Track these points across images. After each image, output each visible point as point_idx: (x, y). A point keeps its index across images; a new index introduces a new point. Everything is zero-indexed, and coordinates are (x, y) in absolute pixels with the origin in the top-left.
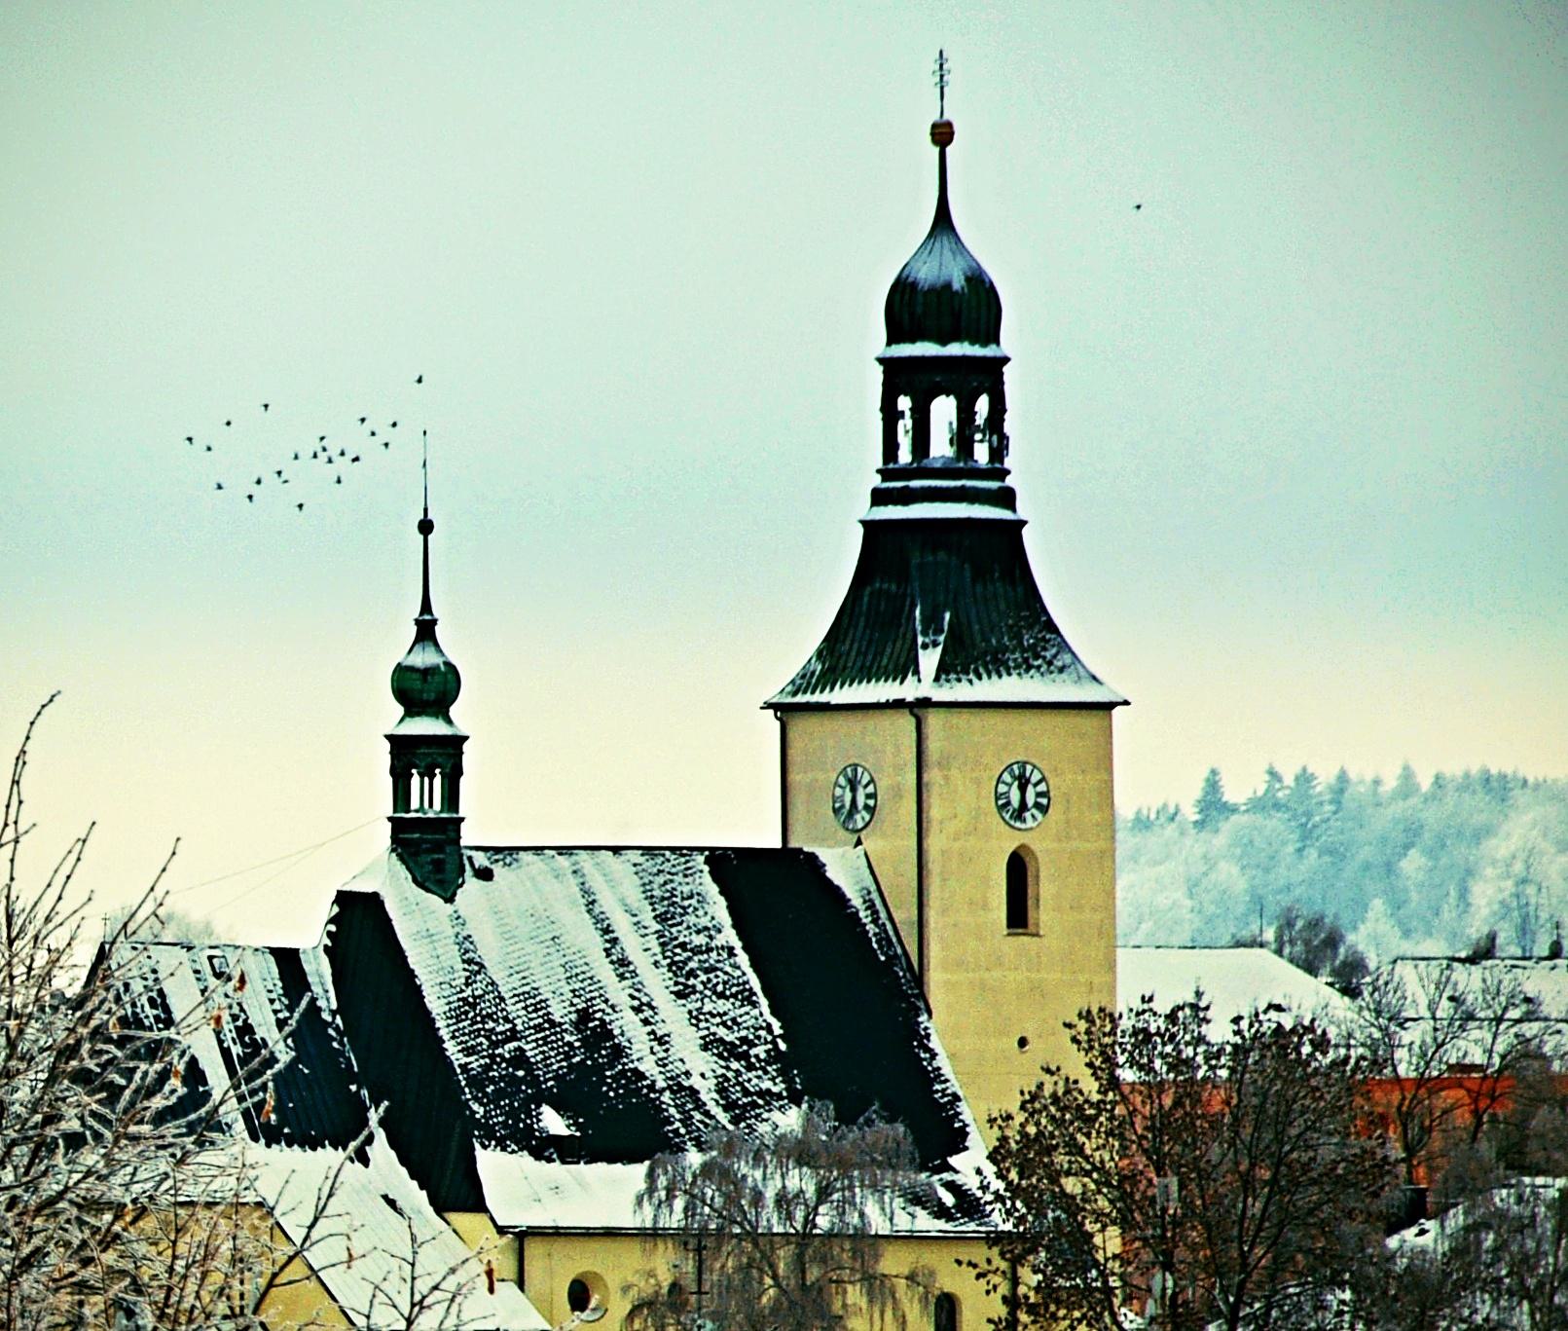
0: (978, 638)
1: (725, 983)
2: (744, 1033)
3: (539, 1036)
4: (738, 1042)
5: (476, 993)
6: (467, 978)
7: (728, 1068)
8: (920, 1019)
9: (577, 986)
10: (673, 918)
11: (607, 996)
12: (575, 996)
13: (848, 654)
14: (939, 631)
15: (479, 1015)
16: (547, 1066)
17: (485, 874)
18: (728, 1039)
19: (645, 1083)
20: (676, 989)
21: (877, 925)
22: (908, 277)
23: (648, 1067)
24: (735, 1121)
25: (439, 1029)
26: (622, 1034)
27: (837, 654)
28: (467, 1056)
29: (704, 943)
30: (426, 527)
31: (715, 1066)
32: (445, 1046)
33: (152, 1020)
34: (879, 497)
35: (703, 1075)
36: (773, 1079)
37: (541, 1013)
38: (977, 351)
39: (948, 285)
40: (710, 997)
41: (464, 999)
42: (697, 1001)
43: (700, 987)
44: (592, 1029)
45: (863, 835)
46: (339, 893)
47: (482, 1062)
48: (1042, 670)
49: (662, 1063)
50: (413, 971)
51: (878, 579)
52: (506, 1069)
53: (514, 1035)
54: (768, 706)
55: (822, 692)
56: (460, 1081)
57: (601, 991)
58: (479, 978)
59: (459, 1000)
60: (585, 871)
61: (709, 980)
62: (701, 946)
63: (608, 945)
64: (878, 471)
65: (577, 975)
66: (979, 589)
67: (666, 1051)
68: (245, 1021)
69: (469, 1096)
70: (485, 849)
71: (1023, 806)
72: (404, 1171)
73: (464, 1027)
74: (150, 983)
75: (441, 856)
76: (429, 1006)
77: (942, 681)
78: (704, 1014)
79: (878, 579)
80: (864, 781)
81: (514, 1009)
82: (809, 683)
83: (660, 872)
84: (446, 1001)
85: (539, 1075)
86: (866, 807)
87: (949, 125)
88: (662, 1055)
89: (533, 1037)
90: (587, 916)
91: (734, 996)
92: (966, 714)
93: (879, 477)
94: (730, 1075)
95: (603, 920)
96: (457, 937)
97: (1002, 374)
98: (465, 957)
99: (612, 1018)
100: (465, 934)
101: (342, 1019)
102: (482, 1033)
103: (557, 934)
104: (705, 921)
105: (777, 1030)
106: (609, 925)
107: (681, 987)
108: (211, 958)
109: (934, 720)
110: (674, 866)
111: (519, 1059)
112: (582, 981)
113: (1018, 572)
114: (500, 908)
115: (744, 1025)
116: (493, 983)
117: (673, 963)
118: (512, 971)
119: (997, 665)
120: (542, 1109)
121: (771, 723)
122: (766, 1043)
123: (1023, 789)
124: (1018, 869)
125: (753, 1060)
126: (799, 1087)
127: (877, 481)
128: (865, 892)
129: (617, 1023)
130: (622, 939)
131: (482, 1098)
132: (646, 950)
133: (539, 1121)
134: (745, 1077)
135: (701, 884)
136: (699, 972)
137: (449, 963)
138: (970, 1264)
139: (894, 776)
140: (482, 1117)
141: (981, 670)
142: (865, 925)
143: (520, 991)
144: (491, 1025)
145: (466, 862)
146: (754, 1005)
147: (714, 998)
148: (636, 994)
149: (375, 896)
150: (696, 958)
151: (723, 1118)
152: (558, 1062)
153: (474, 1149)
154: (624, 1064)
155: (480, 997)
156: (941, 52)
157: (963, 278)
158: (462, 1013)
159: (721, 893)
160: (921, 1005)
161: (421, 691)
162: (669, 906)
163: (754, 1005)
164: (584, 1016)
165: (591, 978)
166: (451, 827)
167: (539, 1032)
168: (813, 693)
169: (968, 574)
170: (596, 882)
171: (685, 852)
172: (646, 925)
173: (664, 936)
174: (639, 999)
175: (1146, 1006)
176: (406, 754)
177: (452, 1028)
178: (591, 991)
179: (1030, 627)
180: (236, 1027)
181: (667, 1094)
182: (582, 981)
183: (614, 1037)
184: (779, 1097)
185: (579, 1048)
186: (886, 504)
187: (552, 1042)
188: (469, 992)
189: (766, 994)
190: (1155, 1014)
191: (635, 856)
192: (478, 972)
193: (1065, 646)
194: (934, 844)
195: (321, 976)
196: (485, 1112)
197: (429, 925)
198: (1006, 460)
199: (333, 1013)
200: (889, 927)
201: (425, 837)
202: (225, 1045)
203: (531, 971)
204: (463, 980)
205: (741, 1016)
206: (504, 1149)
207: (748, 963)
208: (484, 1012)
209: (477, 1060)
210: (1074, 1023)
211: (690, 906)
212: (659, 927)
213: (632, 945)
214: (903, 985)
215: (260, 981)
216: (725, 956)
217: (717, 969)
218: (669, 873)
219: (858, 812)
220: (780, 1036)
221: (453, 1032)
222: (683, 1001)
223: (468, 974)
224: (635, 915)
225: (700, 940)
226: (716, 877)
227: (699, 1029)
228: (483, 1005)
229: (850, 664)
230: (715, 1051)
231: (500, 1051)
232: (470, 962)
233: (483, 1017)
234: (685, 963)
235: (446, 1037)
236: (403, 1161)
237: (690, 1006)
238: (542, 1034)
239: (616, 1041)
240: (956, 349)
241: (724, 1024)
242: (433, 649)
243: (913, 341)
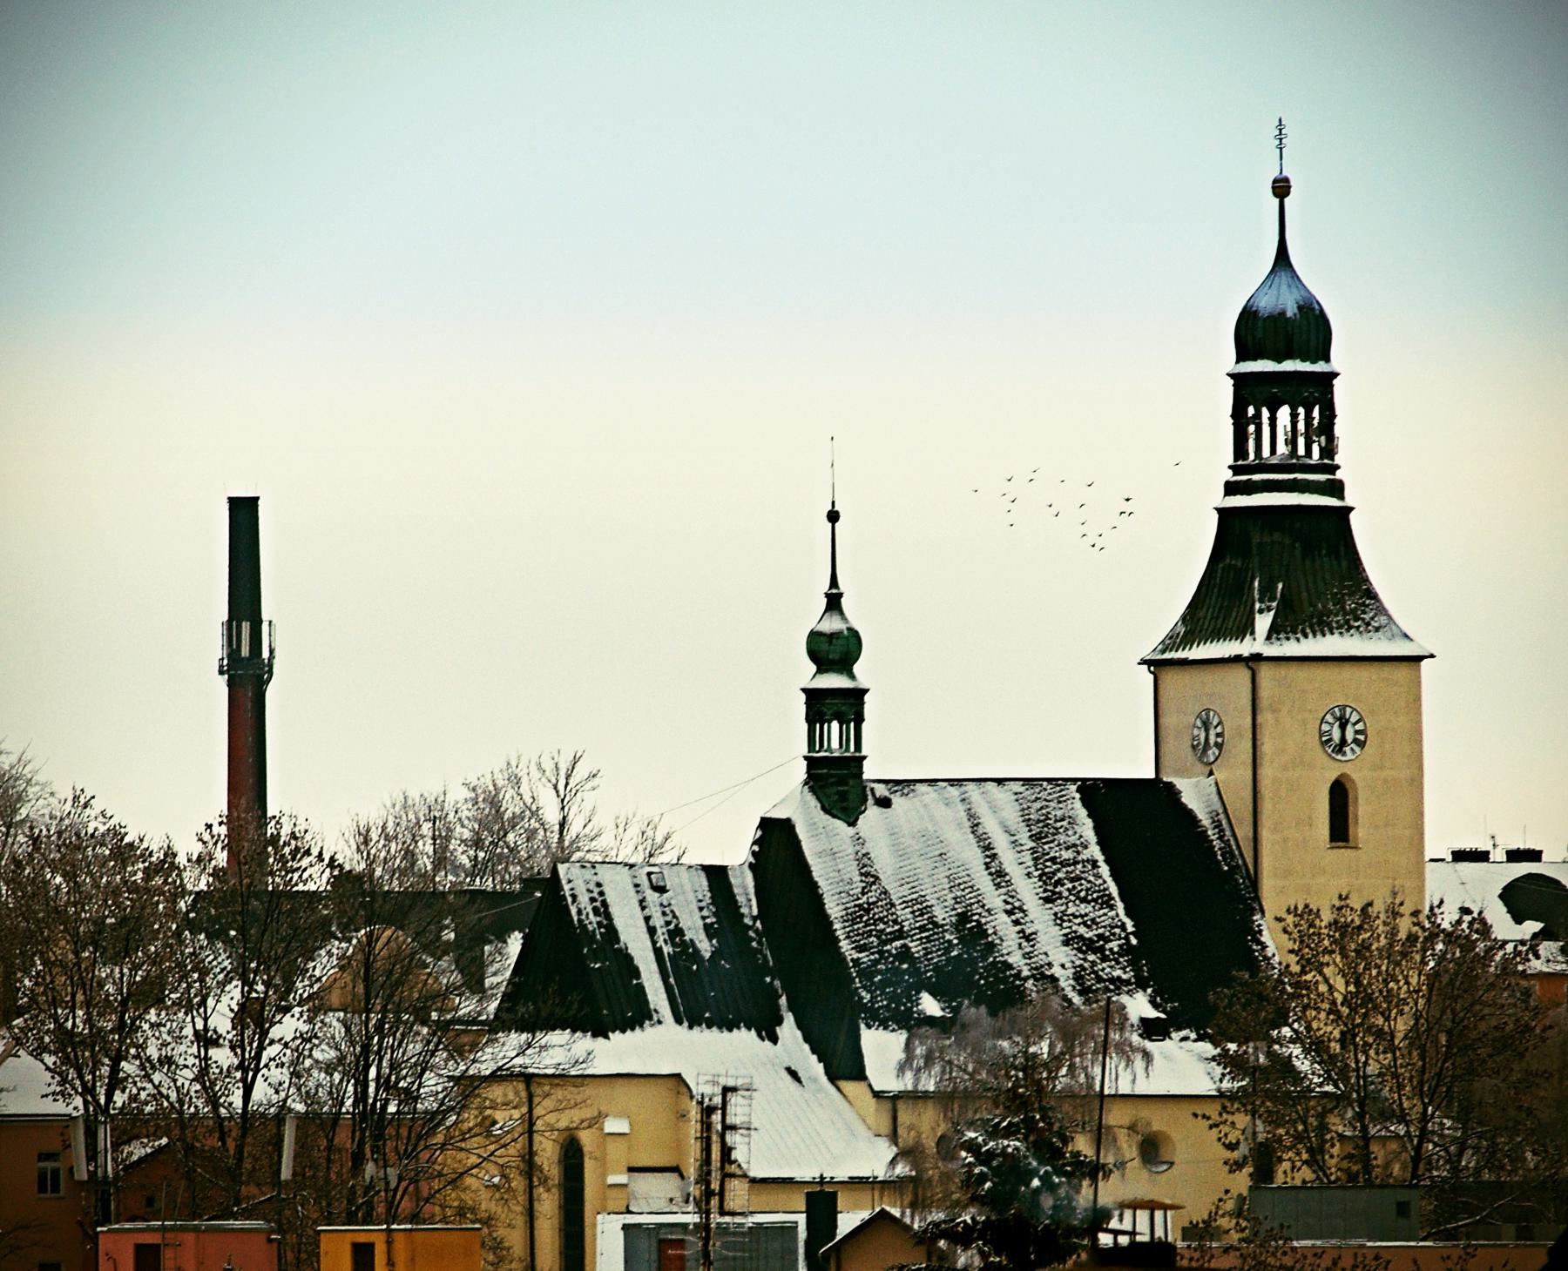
0: (1306, 604)
1: (1087, 890)
2: (1101, 931)
3: (923, 935)
4: (1095, 939)
5: (871, 900)
6: (864, 888)
7: (1085, 960)
8: (1255, 918)
9: (959, 894)
10: (1046, 836)
11: (985, 902)
12: (957, 903)
13: (1205, 618)
14: (1272, 599)
15: (872, 918)
16: (928, 960)
17: (884, 803)
18: (1087, 936)
19: (1012, 972)
20: (1045, 895)
21: (1223, 841)
22: (1252, 306)
23: (1016, 959)
24: (1087, 1002)
25: (836, 930)
26: (995, 933)
27: (1195, 620)
28: (860, 952)
29: (1071, 857)
30: (833, 517)
31: (1074, 959)
32: (841, 944)
33: (595, 926)
34: (1231, 489)
35: (1063, 966)
36: (1123, 969)
37: (926, 917)
38: (1306, 367)
39: (1283, 313)
40: (1074, 902)
41: (859, 906)
42: (1062, 905)
43: (1066, 894)
44: (971, 929)
45: (1213, 767)
46: (763, 819)
47: (872, 957)
48: (1361, 629)
49: (1027, 956)
50: (816, 883)
51: (1228, 556)
52: (893, 962)
53: (900, 934)
54: (1144, 662)
55: (1183, 649)
56: (851, 973)
57: (980, 898)
58: (874, 887)
59: (855, 906)
60: (972, 799)
61: (1074, 887)
62: (1069, 860)
63: (988, 860)
64: (1230, 467)
65: (960, 884)
66: (1308, 563)
67: (1033, 946)
68: (677, 925)
69: (858, 985)
70: (886, 782)
71: (1343, 741)
72: (807, 1047)
73: (859, 929)
74: (595, 895)
75: (846, 788)
76: (829, 911)
77: (1273, 640)
78: (1068, 915)
79: (1228, 556)
80: (1215, 723)
81: (904, 914)
82: (1175, 642)
83: (1037, 799)
84: (844, 907)
85: (920, 967)
86: (1216, 744)
87: (1286, 180)
88: (1028, 949)
89: (918, 936)
90: (972, 836)
91: (1095, 900)
92: (1294, 666)
93: (1230, 472)
94: (1086, 965)
95: (986, 839)
96: (857, 853)
97: (1333, 386)
98: (863, 871)
99: (988, 919)
100: (864, 851)
101: (762, 923)
102: (874, 933)
103: (943, 851)
104: (1073, 839)
105: (1130, 928)
106: (990, 843)
107: (1050, 894)
108: (649, 874)
109: (1266, 673)
110: (1050, 794)
111: (905, 954)
112: (963, 890)
113: (1342, 548)
114: (896, 830)
115: (1103, 924)
116: (885, 893)
117: (1044, 874)
118: (903, 882)
119: (1321, 626)
120: (921, 995)
121: (1146, 677)
122: (1120, 939)
123: (1343, 727)
124: (1340, 794)
125: (1107, 953)
126: (1146, 974)
127: (1228, 475)
128: (1214, 813)
129: (993, 924)
130: (1000, 854)
131: (871, 986)
132: (1021, 864)
133: (918, 1005)
134: (1100, 967)
135: (1072, 809)
136: (1066, 881)
137: (848, 876)
138: (1204, 1116)
139: (1237, 720)
140: (869, 1002)
141: (1308, 631)
142: (1213, 841)
143: (910, 898)
144: (881, 926)
145: (869, 793)
146: (1112, 907)
147: (1077, 902)
148: (1010, 900)
149: (788, 820)
150: (1064, 870)
151: (1077, 1000)
152: (939, 956)
153: (859, 1029)
154: (995, 957)
155: (874, 903)
156: (1280, 120)
157: (1295, 306)
158: (858, 917)
159: (1089, 816)
160: (1256, 906)
161: (828, 652)
162: (1043, 827)
163: (1112, 907)
164: (964, 918)
165: (972, 887)
166: (853, 764)
167: (924, 932)
168: (1177, 651)
169: (1298, 552)
170: (982, 809)
171: (1060, 782)
172: (1023, 842)
173: (1036, 852)
174: (1012, 904)
175: (1343, 903)
176: (820, 706)
177: (848, 929)
178: (971, 898)
179: (1352, 594)
180: (668, 931)
181: (1031, 981)
182: (963, 890)
183: (988, 935)
184: (1128, 982)
185: (957, 945)
186: (1234, 494)
187: (934, 940)
188: (864, 899)
189: (1123, 900)
190: (1352, 909)
191: (1017, 787)
192: (874, 883)
193: (1381, 610)
194: (1266, 772)
195: (745, 888)
196: (872, 997)
197: (833, 845)
198: (1336, 457)
199: (754, 919)
200: (1232, 842)
201: (832, 772)
202: (658, 945)
203: (920, 882)
204: (860, 890)
205: (1099, 917)
206: (885, 1028)
207: (1109, 873)
208: (877, 916)
209: (868, 956)
210: (1283, 917)
211: (1062, 827)
212: (1034, 844)
213: (1008, 859)
214: (1242, 890)
215: (692, 893)
216: (1090, 867)
217: (1082, 878)
218: (1045, 800)
219: (1211, 748)
220: (1132, 933)
221: (849, 932)
222: (1051, 905)
223: (864, 885)
224: (1014, 835)
225: (1067, 855)
226: (1086, 803)
227: (1062, 928)
228: (876, 910)
229: (1205, 627)
230: (1075, 946)
231: (888, 947)
232: (867, 875)
233: (875, 920)
234: (1054, 873)
235: (842, 937)
236: (806, 1039)
237: (1056, 909)
238: (927, 934)
239: (990, 939)
240: (1289, 366)
241: (1084, 923)
242: (839, 617)
243: (1255, 359)
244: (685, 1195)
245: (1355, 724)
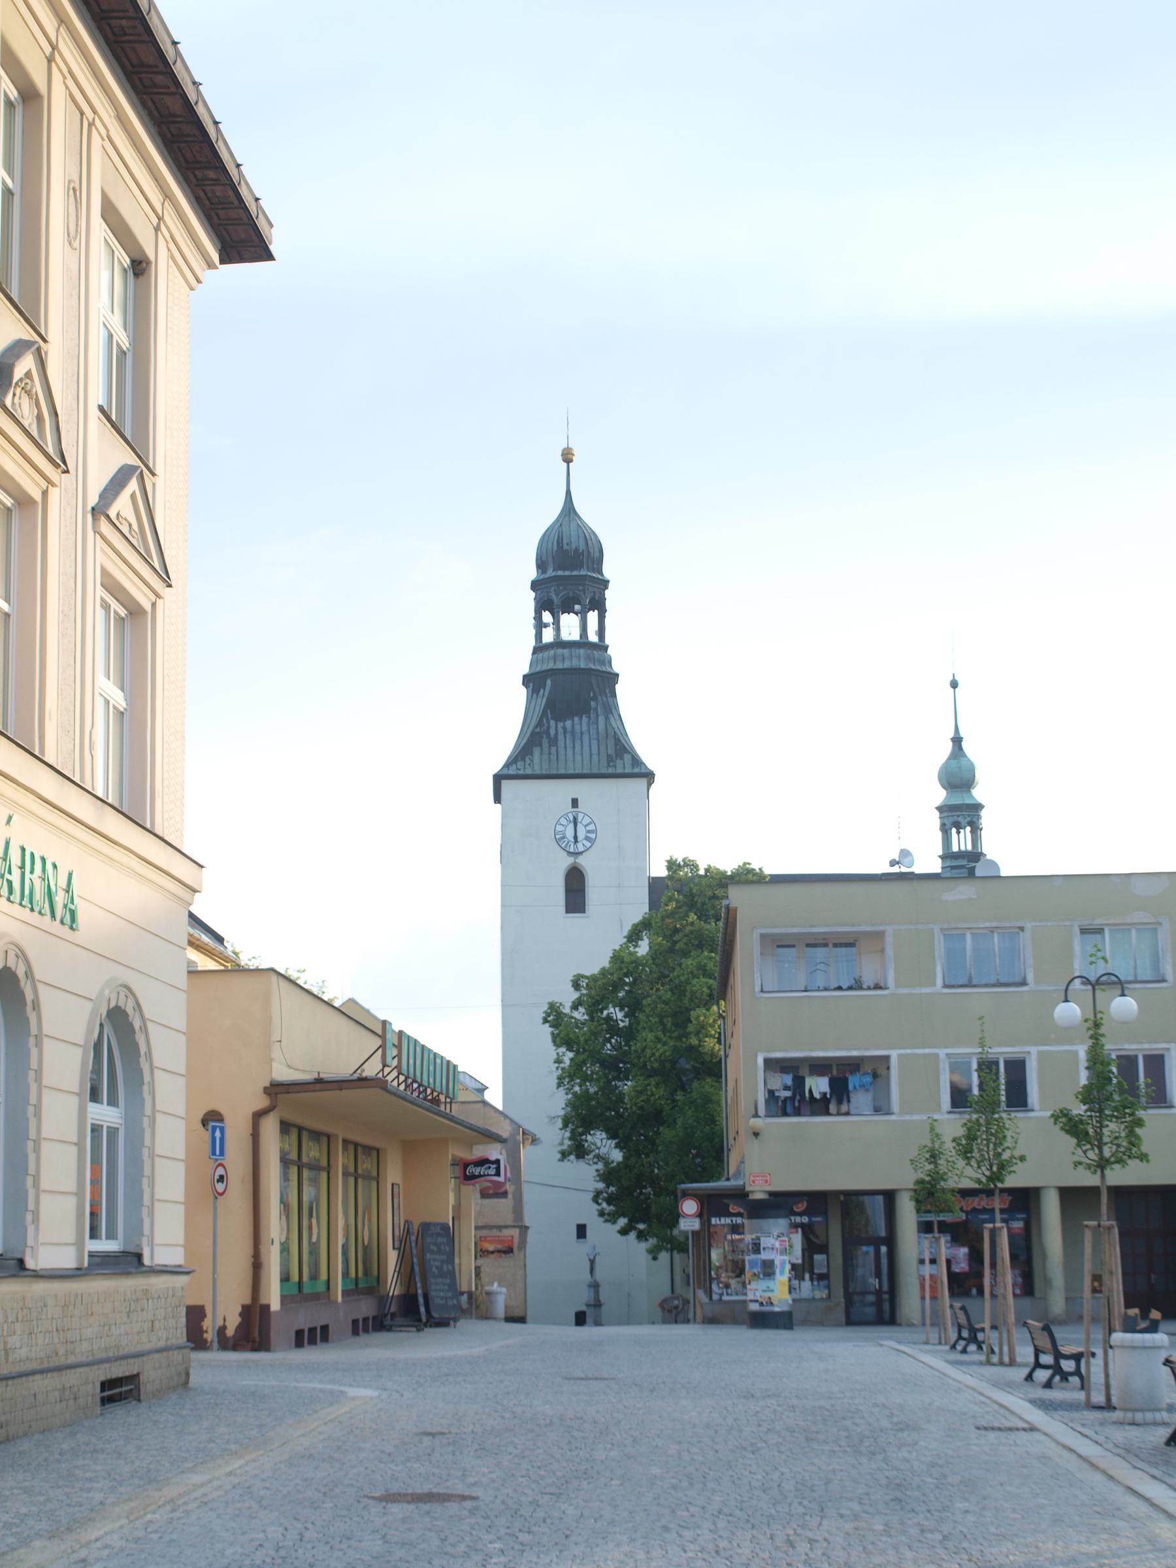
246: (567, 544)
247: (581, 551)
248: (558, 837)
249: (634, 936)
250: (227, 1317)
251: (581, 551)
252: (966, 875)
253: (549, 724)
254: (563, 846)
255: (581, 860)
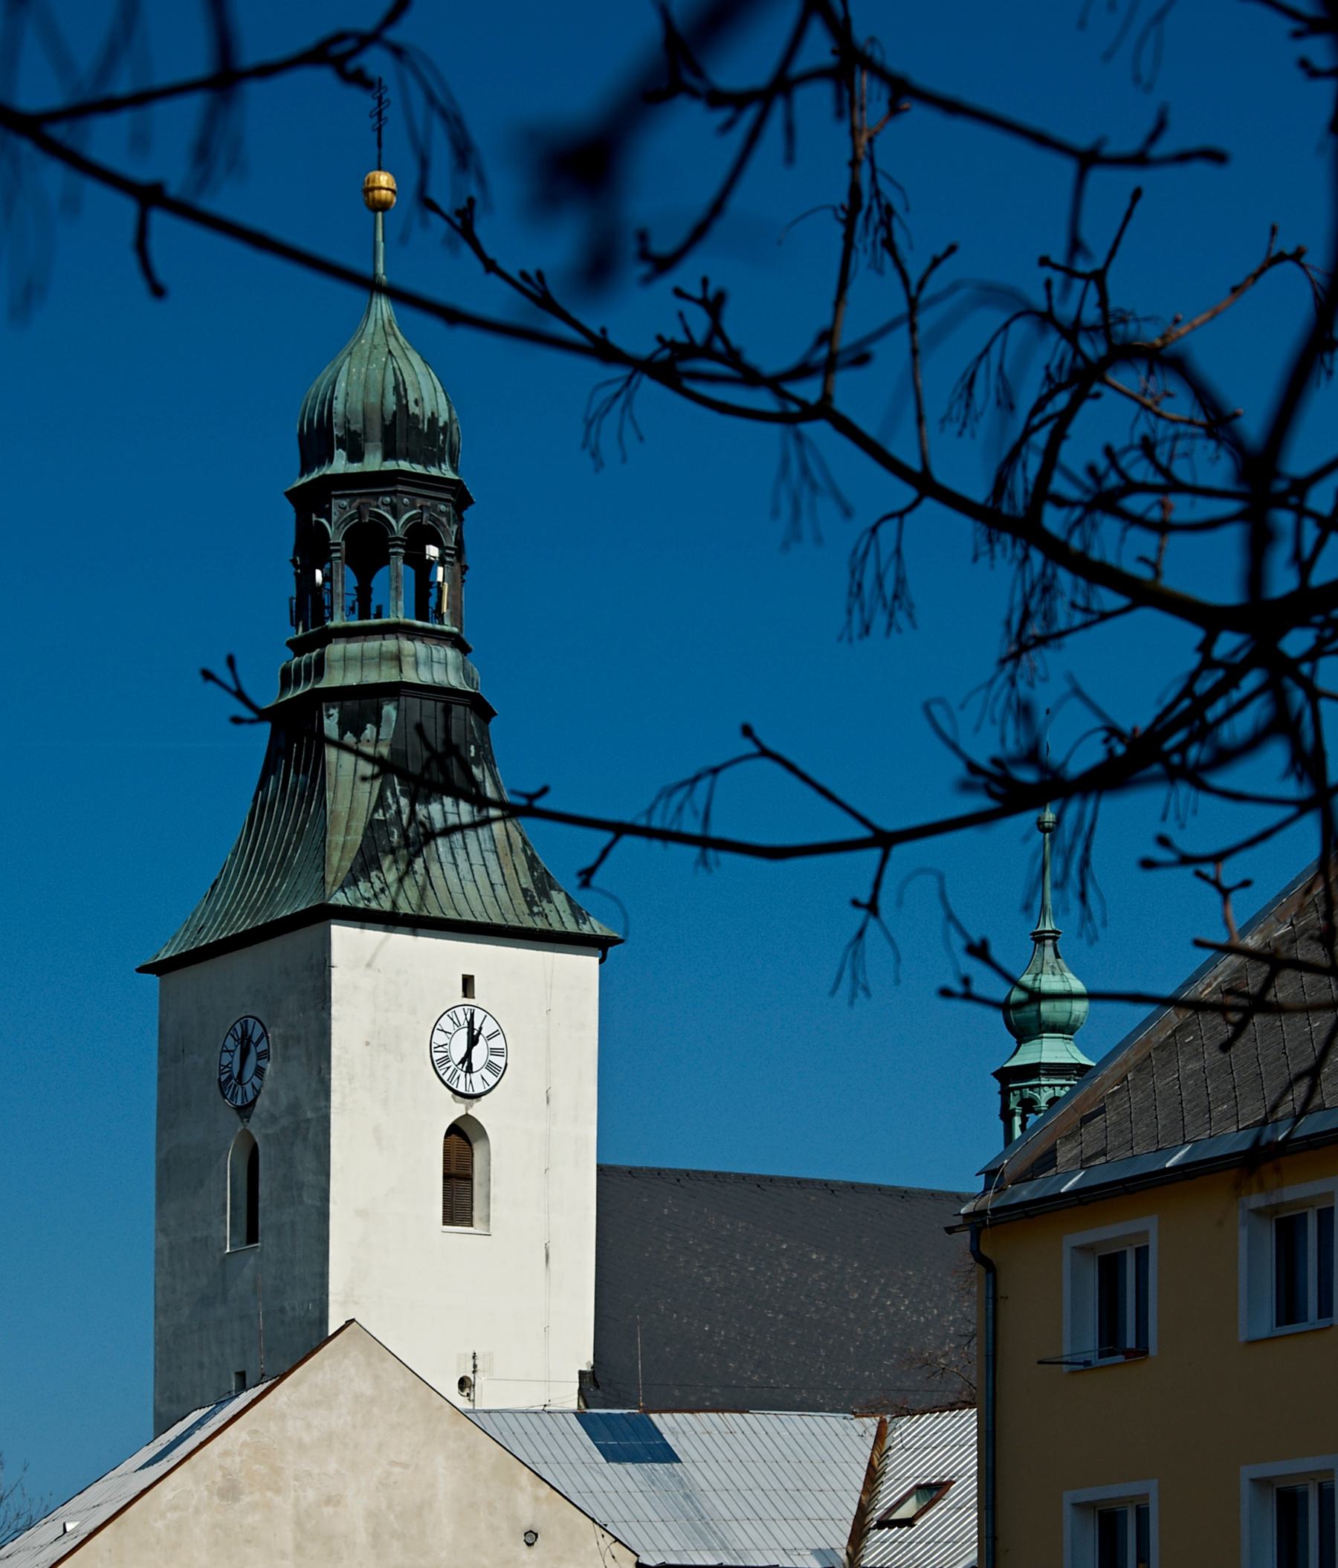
244: (998, 1195)
245: (490, 1037)
246: (416, 402)
247: (441, 424)
248: (436, 1056)
249: (907, 110)
250: (1173, 117)
251: (441, 424)
252: (1324, 1484)
253: (398, 803)
254: (445, 1078)
255: (477, 1110)
